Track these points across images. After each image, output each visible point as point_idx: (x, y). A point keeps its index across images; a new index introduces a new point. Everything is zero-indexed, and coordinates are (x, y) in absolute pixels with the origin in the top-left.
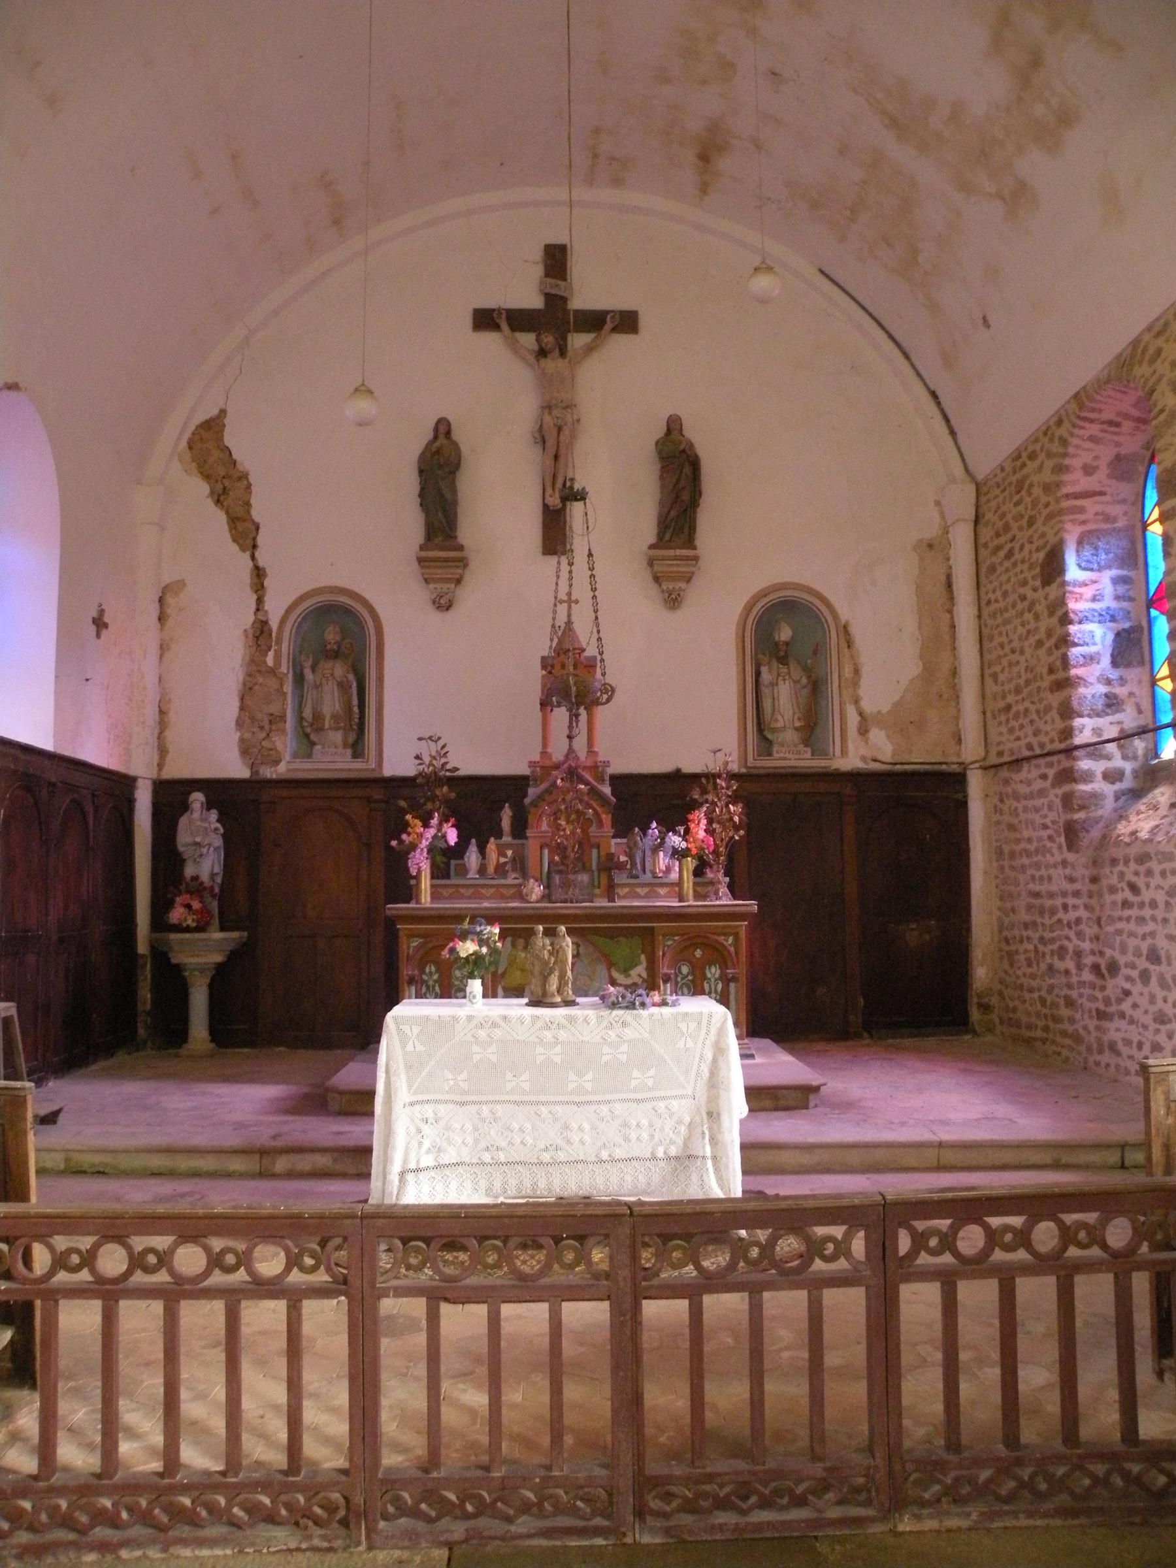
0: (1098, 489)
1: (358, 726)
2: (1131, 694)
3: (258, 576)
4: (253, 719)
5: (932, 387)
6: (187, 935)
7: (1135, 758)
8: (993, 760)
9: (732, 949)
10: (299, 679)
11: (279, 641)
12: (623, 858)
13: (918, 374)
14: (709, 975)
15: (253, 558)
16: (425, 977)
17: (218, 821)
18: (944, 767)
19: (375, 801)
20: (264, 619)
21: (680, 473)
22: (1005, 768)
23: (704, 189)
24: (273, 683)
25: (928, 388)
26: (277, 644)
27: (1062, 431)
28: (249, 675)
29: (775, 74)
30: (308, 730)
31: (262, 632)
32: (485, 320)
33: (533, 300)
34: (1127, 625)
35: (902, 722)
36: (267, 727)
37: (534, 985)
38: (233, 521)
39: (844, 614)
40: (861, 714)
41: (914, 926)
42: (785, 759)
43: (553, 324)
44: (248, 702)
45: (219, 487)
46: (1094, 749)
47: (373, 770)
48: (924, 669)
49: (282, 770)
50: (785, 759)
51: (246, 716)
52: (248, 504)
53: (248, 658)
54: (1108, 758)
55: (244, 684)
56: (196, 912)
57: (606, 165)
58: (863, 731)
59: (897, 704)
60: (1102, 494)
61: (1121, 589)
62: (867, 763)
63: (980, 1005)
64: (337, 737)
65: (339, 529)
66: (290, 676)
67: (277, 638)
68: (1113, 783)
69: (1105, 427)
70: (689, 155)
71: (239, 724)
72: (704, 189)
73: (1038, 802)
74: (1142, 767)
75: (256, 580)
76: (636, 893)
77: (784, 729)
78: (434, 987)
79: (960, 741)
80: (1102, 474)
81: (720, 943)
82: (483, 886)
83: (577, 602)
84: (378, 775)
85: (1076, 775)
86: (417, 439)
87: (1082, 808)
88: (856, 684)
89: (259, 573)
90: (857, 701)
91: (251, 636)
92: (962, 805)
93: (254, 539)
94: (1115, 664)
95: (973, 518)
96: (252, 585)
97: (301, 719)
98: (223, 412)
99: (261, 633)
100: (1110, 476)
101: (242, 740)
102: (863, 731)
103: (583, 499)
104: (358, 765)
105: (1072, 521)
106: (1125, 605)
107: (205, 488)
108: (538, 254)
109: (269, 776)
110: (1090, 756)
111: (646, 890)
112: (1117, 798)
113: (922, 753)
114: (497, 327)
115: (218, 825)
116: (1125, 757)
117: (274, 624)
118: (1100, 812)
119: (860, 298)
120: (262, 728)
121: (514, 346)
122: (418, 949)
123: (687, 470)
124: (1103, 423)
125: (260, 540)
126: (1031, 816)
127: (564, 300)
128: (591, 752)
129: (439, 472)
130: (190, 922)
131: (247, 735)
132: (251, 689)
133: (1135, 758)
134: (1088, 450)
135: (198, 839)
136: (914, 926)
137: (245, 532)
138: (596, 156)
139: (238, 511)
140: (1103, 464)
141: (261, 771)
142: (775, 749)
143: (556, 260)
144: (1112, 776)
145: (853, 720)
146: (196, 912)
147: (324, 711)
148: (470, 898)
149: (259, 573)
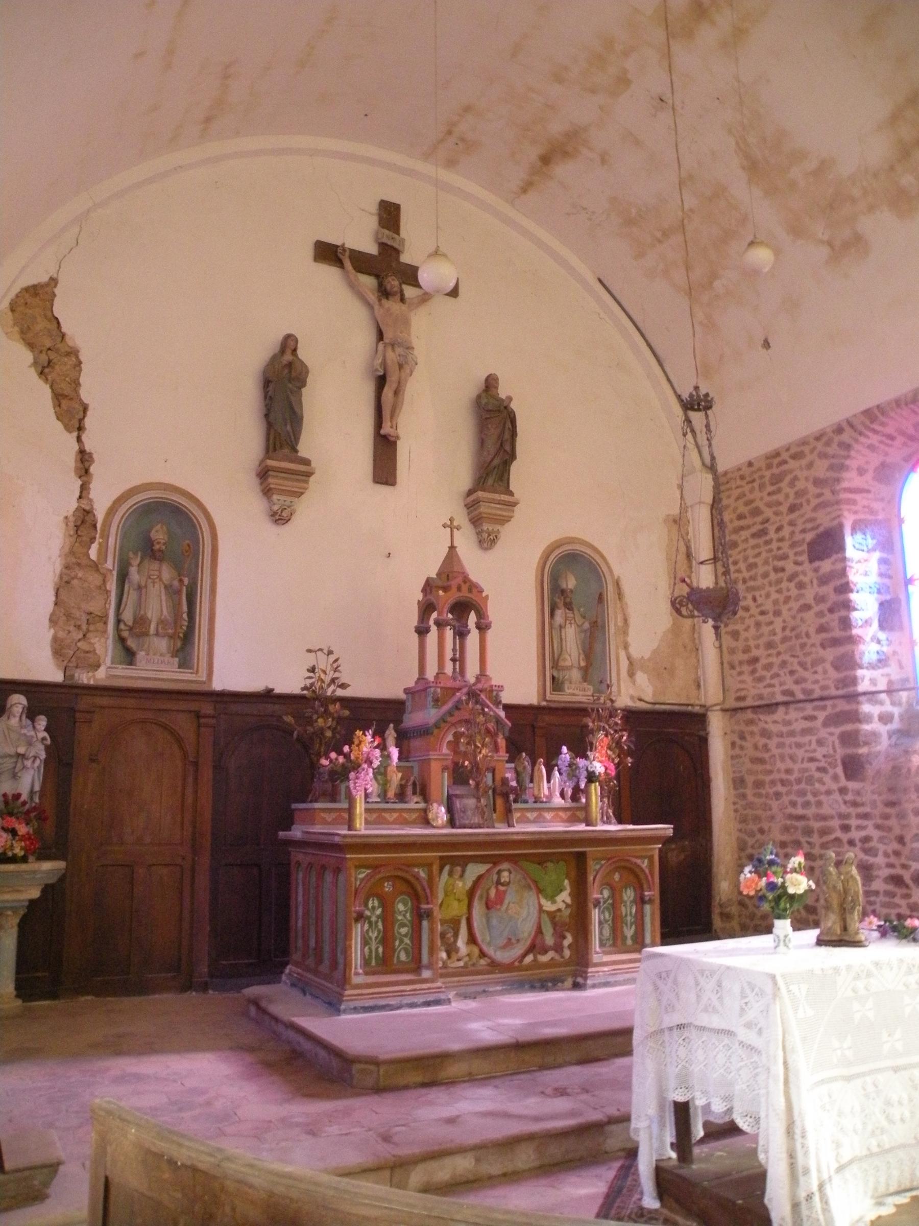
0: (866, 487)
1: (185, 639)
2: (895, 653)
3: (82, 461)
4: (69, 616)
5: (679, 392)
6: (11, 867)
7: (900, 704)
8: (731, 703)
9: (647, 871)
10: (123, 577)
11: (105, 536)
12: (514, 784)
13: (669, 380)
14: (625, 898)
15: (79, 439)
16: (368, 913)
17: (46, 730)
18: (690, 708)
19: (205, 716)
20: (87, 508)
21: (495, 426)
22: (749, 711)
23: (526, 188)
24: (94, 579)
25: (675, 392)
26: (102, 537)
27: (845, 437)
28: (67, 567)
29: (662, 100)
30: (125, 634)
31: (83, 522)
32: (327, 253)
33: (372, 249)
34: (888, 597)
35: (661, 669)
36: (84, 627)
37: (831, 921)
38: (58, 397)
39: (617, 570)
40: (629, 658)
41: (673, 846)
42: (574, 695)
43: (383, 271)
44: (63, 595)
45: (44, 358)
46: (871, 695)
47: (204, 683)
48: (674, 624)
49: (100, 676)
50: (574, 695)
51: (62, 612)
52: (76, 384)
53: (67, 549)
54: (881, 703)
55: (61, 577)
56: (23, 838)
57: (453, 145)
58: (631, 674)
59: (655, 652)
60: (868, 491)
61: (884, 568)
62: (635, 702)
63: (722, 915)
64: (162, 644)
65: (177, 430)
66: (115, 573)
67: (103, 530)
68: (886, 724)
69: (884, 439)
70: (533, 153)
71: (53, 621)
72: (526, 188)
73: (806, 739)
74: (907, 711)
75: (79, 465)
76: (385, 819)
77: (570, 668)
78: (377, 922)
79: (699, 686)
80: (869, 476)
81: (638, 866)
82: (384, 810)
83: (444, 526)
84: (205, 688)
85: (861, 716)
86: (257, 354)
87: (866, 743)
88: (625, 633)
89: (84, 460)
90: (626, 647)
91: (71, 524)
92: (704, 741)
93: (81, 420)
94: (882, 627)
95: (711, 502)
96: (77, 469)
97: (118, 621)
98: (54, 281)
99: (83, 523)
100: (874, 478)
101: (55, 639)
102: (631, 674)
103: (708, 407)
104: (186, 676)
105: (849, 510)
106: (886, 581)
107: (27, 356)
108: (374, 208)
109: (85, 682)
110: (870, 701)
111: (535, 814)
112: (890, 737)
113: (673, 695)
114: (339, 263)
115: (46, 734)
116: (893, 704)
117: (100, 516)
118: (878, 748)
119: (631, 313)
120: (79, 627)
121: (353, 286)
122: (417, 878)
123: (509, 425)
124: (884, 435)
125: (87, 422)
126: (794, 750)
127: (397, 252)
128: (482, 674)
129: (282, 386)
130: (18, 851)
131: (61, 634)
132: (68, 582)
133: (900, 704)
134: (864, 455)
135: (21, 750)
136: (673, 846)
137: (71, 411)
138: (450, 133)
139: (66, 389)
140: (871, 468)
141: (76, 675)
142: (566, 685)
143: (389, 215)
144: (885, 718)
145: (624, 664)
146: (23, 838)
147: (149, 615)
148: (394, 823)
149: (84, 460)
